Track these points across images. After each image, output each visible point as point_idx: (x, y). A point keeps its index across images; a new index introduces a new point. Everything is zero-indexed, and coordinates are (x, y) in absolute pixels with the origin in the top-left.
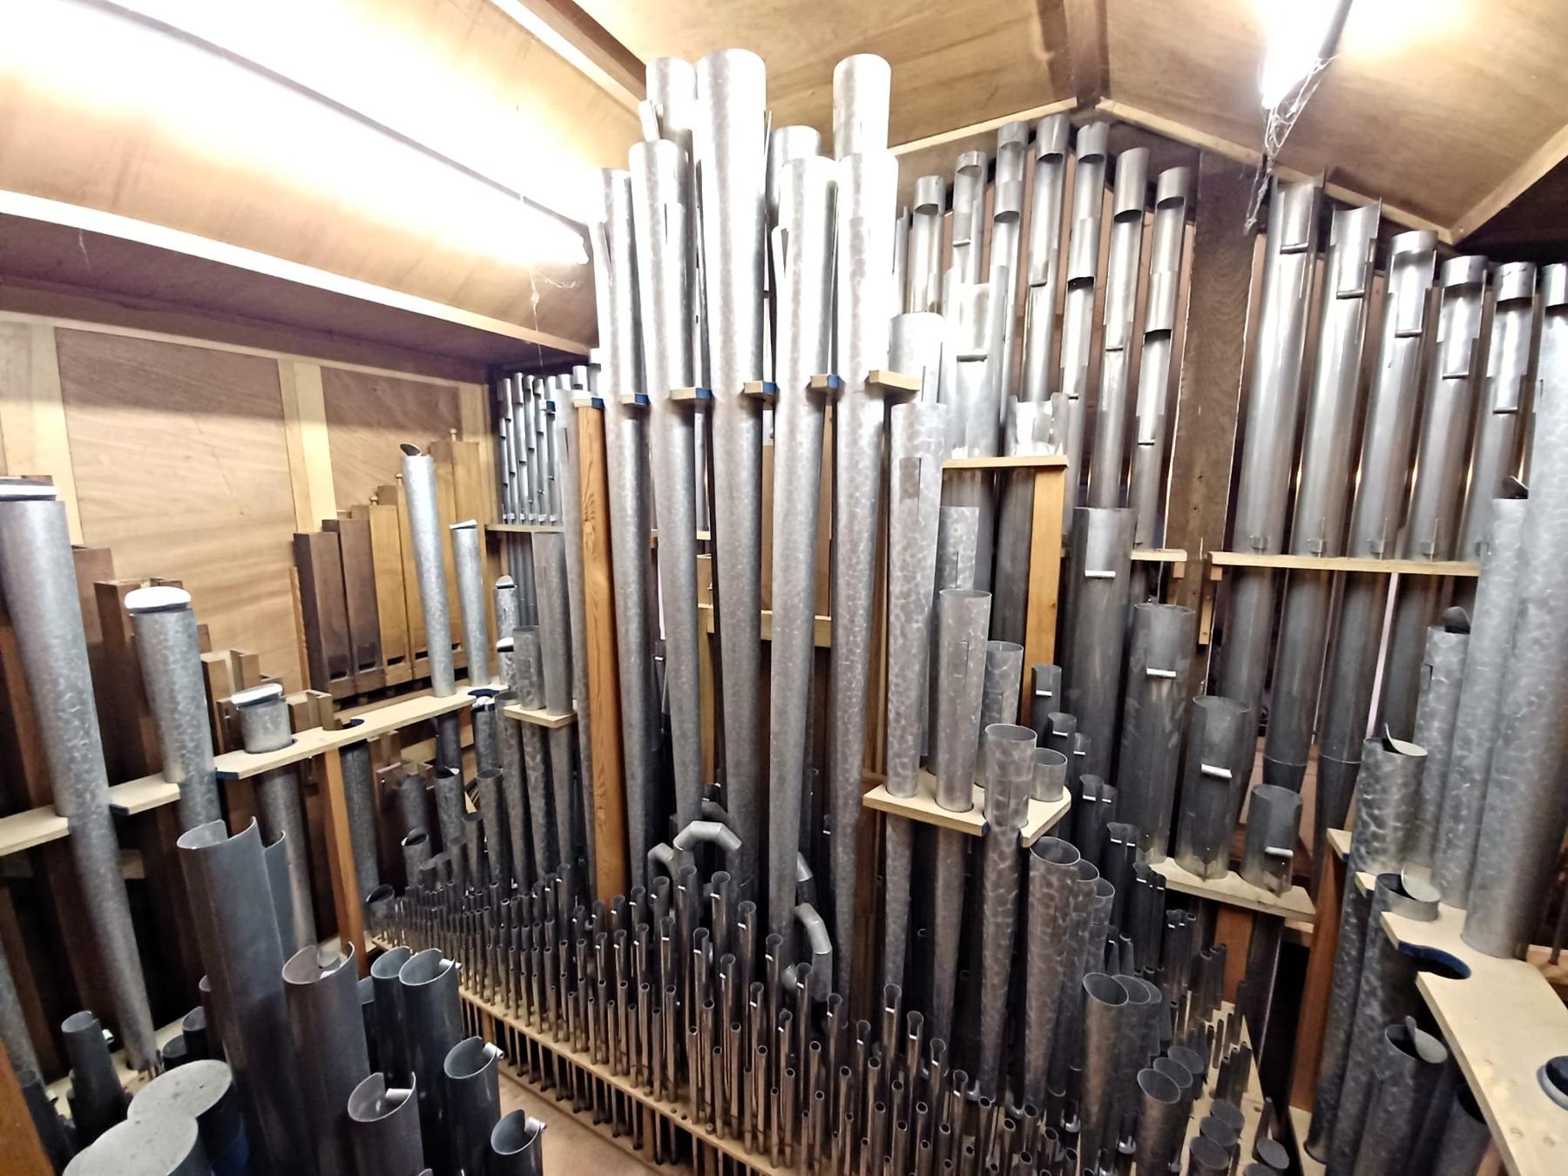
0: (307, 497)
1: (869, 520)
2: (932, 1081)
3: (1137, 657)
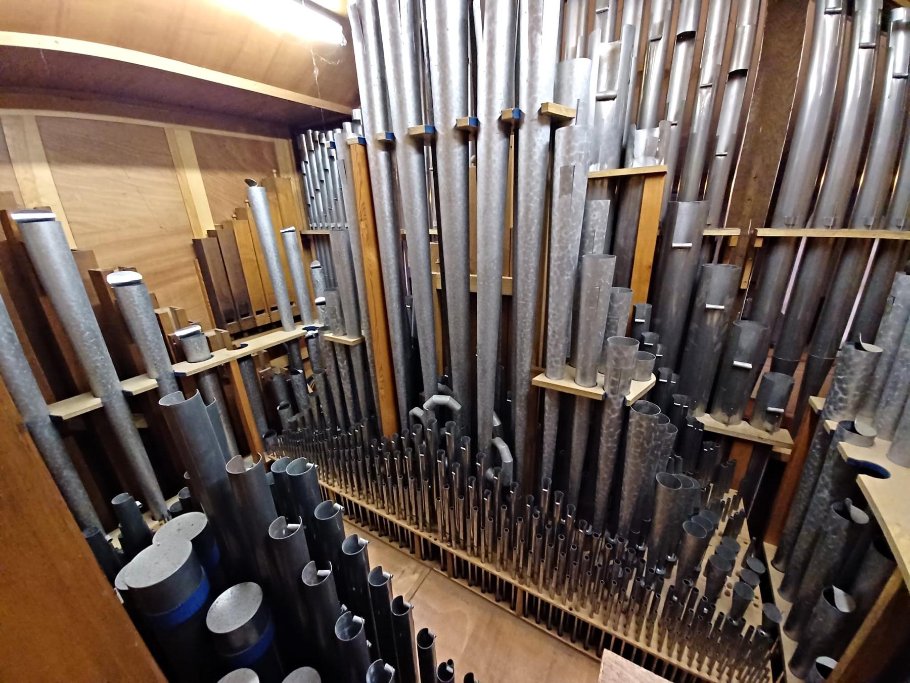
0: (196, 217)
1: (538, 211)
2: (568, 525)
3: (700, 297)
